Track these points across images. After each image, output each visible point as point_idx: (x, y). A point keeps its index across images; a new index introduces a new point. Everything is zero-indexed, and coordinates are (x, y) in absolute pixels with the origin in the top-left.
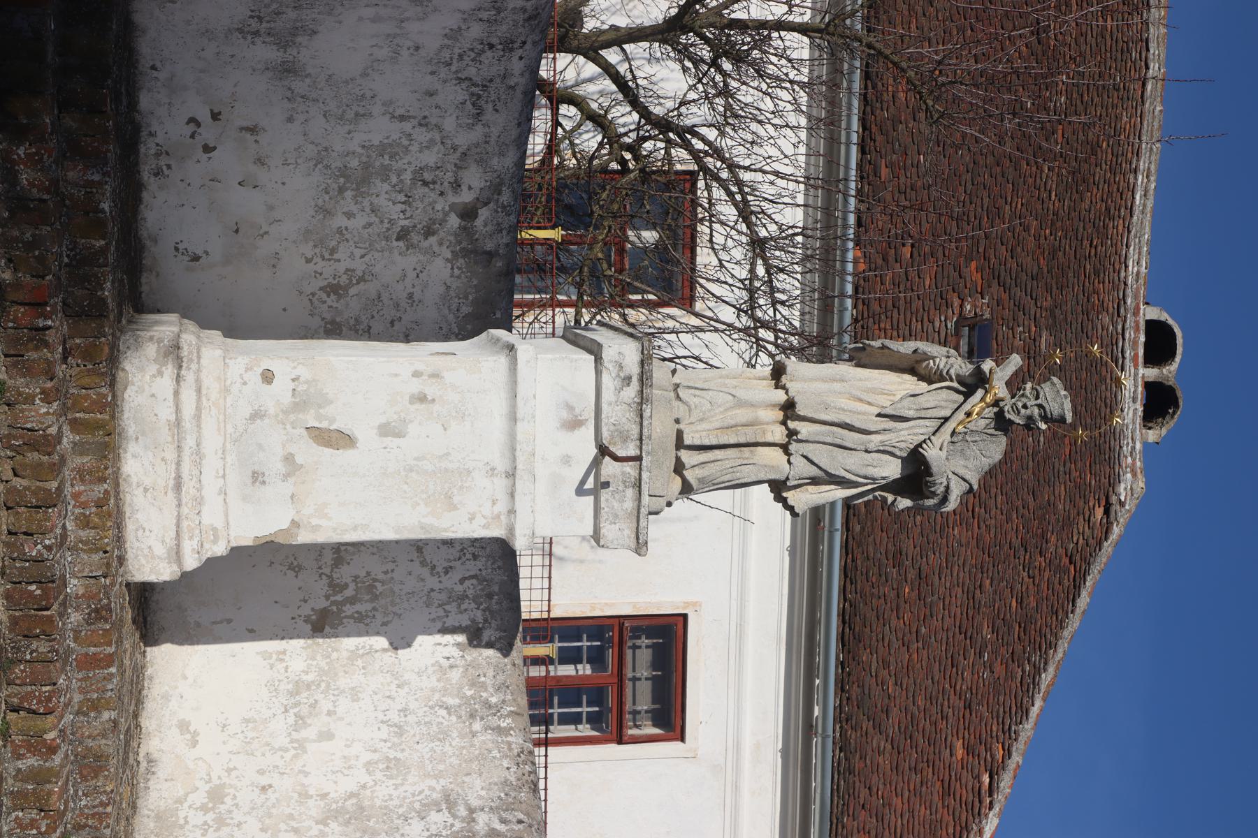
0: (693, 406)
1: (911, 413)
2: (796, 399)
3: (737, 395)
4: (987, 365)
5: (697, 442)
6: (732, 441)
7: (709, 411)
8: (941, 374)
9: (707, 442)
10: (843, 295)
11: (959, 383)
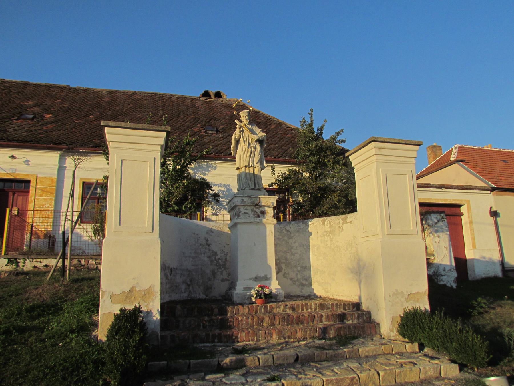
1: (247, 142)
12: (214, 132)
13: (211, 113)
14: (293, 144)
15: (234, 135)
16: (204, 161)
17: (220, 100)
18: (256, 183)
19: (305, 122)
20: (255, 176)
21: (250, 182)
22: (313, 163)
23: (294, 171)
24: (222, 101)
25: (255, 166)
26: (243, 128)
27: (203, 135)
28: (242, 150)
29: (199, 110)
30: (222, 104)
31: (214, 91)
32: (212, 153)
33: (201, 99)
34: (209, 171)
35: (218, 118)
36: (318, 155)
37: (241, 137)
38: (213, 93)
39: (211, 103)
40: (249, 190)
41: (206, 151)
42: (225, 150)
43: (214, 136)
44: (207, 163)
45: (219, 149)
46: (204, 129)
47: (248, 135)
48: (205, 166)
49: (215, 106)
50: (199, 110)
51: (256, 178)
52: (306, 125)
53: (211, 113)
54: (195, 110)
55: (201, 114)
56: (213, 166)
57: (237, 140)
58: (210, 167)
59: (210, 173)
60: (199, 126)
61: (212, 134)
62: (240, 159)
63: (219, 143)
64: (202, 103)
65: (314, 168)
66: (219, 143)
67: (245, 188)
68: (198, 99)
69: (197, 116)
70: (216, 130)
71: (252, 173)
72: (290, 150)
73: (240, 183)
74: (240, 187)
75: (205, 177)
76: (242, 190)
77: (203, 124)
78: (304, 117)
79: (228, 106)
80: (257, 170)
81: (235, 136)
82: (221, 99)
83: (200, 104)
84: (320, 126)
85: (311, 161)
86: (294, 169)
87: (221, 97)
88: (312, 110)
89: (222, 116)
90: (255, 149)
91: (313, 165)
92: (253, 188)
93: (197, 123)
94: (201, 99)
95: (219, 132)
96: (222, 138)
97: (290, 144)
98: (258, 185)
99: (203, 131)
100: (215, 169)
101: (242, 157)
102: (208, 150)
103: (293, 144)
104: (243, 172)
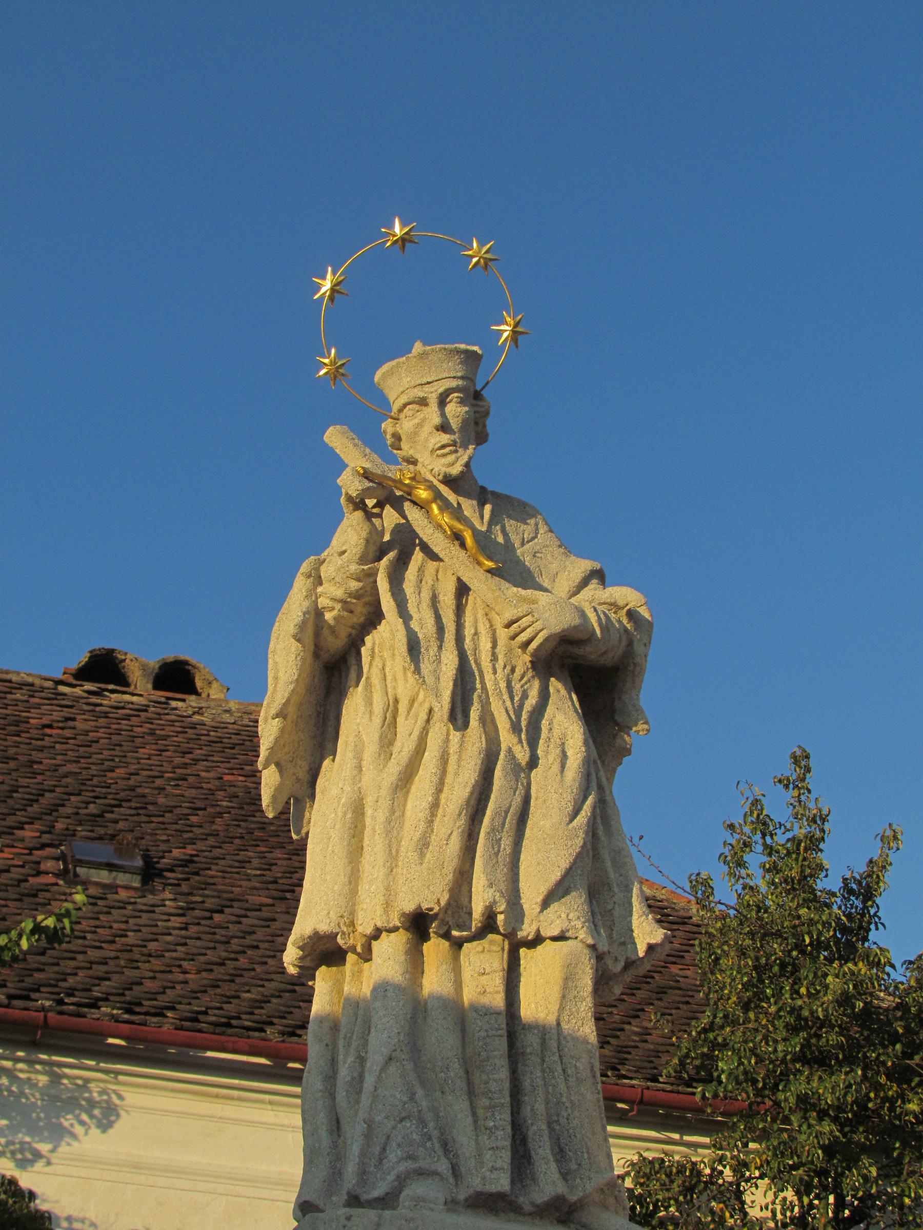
0: (410, 1165)
1: (450, 661)
2: (409, 907)
3: (385, 1051)
4: (349, 483)
5: (505, 1158)
6: (503, 1074)
7: (422, 1122)
8: (357, 595)
9: (504, 1138)
10: (113, 1009)
11: (379, 559)
12: (122, 878)
13: (121, 772)
14: (661, 991)
15: (300, 585)
16: (30, 1062)
17: (184, 705)
18: (538, 1131)
19: (764, 825)
20: (531, 1042)
21: (459, 1107)
22: (822, 1115)
23: (681, 1169)
24: (199, 711)
25: (527, 931)
26: (414, 515)
27: (46, 888)
28: (387, 740)
29: (41, 749)
30: (193, 726)
31: (153, 661)
32: (94, 1005)
33: (63, 689)
34: (58, 1133)
35: (161, 800)
36: (850, 1060)
37: (375, 617)
38: (144, 667)
39: (127, 717)
40: (452, 1205)
41: (37, 929)
42: (195, 994)
43: (123, 905)
44: (56, 1078)
45: (149, 985)
46: (62, 857)
47: (462, 590)
48: (36, 1098)
49: (152, 733)
50: (41, 749)
51: (532, 1077)
52: (770, 850)
53: (121, 772)
54: (17, 745)
55: (55, 769)
56: (92, 1104)
57: (335, 644)
58: (72, 1104)
59: (63, 1148)
60: (29, 833)
61: (113, 888)
62: (355, 851)
63: (153, 946)
64: (66, 712)
65: (829, 1151)
66: (153, 946)
67: (402, 1182)
68: (43, 689)
69: (23, 782)
70: (139, 862)
71: (483, 1012)
72: (646, 1032)
73: (336, 1126)
74: (336, 1173)
75: (26, 1180)
76: (354, 1201)
77: (59, 826)
78: (757, 791)
79: (235, 739)
80: (556, 973)
81: (312, 594)
82: (192, 700)
83: (57, 716)
84: (861, 868)
85: (805, 1103)
86: (678, 1154)
87: (193, 690)
88: (801, 760)
89: (193, 793)
90: (533, 742)
91: (827, 1127)
92: (502, 1183)
93: (20, 817)
94: (63, 689)
95: (157, 883)
96: (176, 922)
97: (641, 994)
98: (560, 1154)
99: (49, 865)
100: (105, 1125)
101: (375, 817)
102: (50, 922)
103: (661, 991)
104: (381, 989)
